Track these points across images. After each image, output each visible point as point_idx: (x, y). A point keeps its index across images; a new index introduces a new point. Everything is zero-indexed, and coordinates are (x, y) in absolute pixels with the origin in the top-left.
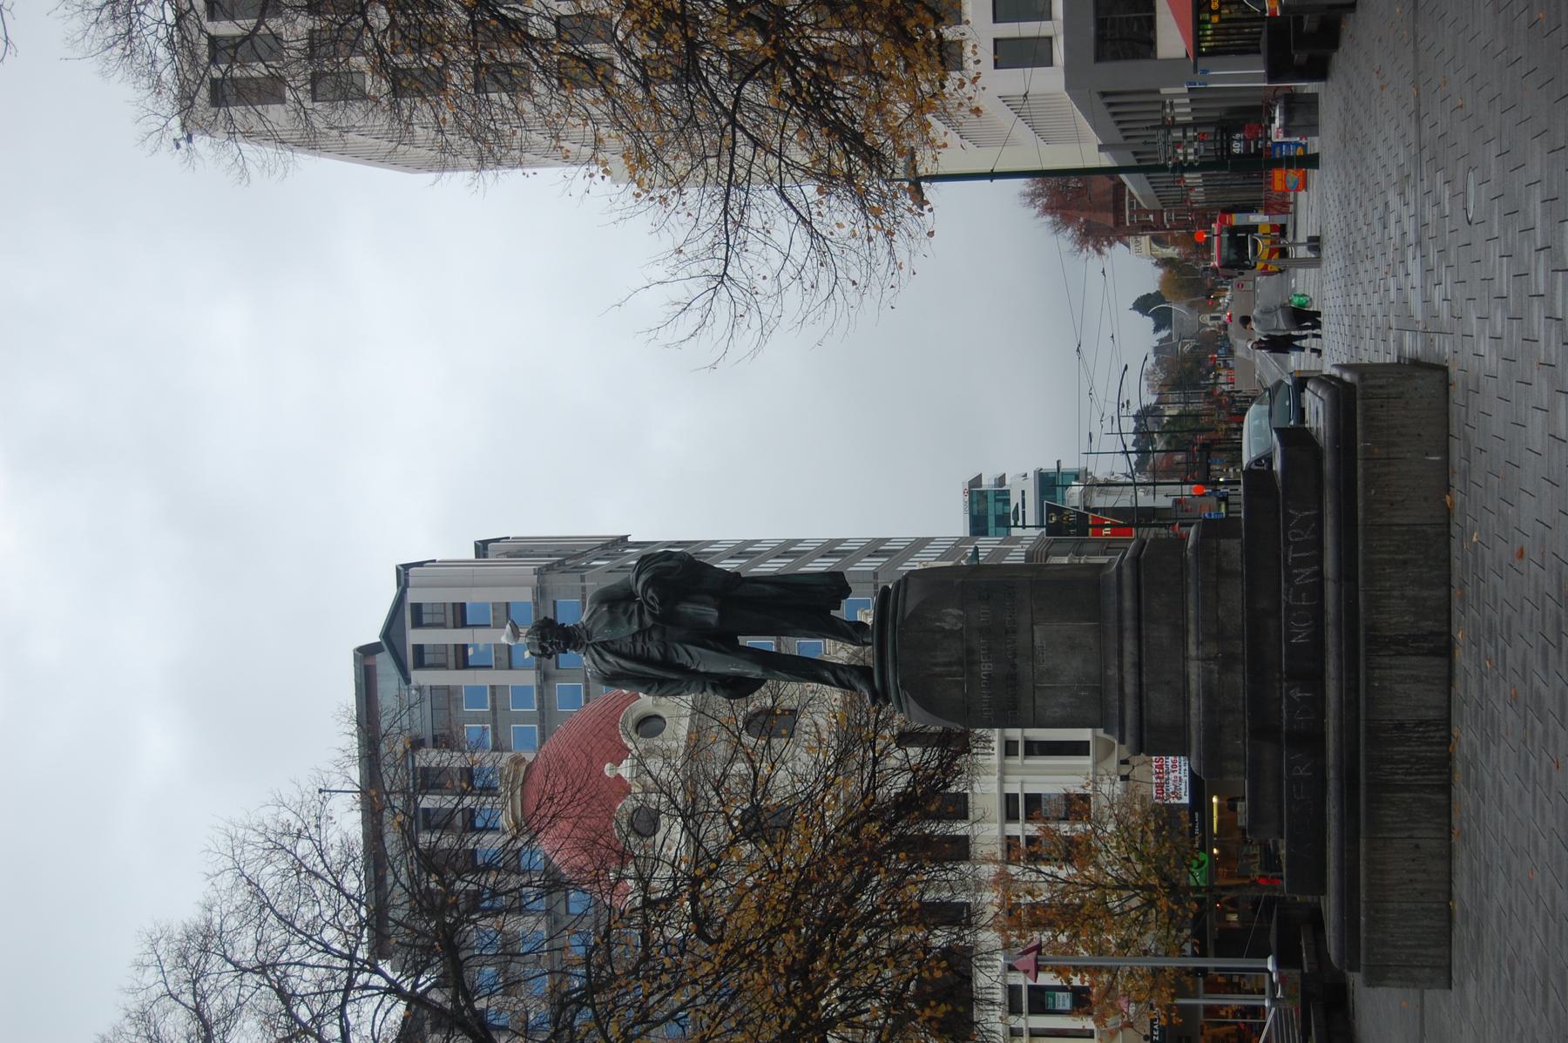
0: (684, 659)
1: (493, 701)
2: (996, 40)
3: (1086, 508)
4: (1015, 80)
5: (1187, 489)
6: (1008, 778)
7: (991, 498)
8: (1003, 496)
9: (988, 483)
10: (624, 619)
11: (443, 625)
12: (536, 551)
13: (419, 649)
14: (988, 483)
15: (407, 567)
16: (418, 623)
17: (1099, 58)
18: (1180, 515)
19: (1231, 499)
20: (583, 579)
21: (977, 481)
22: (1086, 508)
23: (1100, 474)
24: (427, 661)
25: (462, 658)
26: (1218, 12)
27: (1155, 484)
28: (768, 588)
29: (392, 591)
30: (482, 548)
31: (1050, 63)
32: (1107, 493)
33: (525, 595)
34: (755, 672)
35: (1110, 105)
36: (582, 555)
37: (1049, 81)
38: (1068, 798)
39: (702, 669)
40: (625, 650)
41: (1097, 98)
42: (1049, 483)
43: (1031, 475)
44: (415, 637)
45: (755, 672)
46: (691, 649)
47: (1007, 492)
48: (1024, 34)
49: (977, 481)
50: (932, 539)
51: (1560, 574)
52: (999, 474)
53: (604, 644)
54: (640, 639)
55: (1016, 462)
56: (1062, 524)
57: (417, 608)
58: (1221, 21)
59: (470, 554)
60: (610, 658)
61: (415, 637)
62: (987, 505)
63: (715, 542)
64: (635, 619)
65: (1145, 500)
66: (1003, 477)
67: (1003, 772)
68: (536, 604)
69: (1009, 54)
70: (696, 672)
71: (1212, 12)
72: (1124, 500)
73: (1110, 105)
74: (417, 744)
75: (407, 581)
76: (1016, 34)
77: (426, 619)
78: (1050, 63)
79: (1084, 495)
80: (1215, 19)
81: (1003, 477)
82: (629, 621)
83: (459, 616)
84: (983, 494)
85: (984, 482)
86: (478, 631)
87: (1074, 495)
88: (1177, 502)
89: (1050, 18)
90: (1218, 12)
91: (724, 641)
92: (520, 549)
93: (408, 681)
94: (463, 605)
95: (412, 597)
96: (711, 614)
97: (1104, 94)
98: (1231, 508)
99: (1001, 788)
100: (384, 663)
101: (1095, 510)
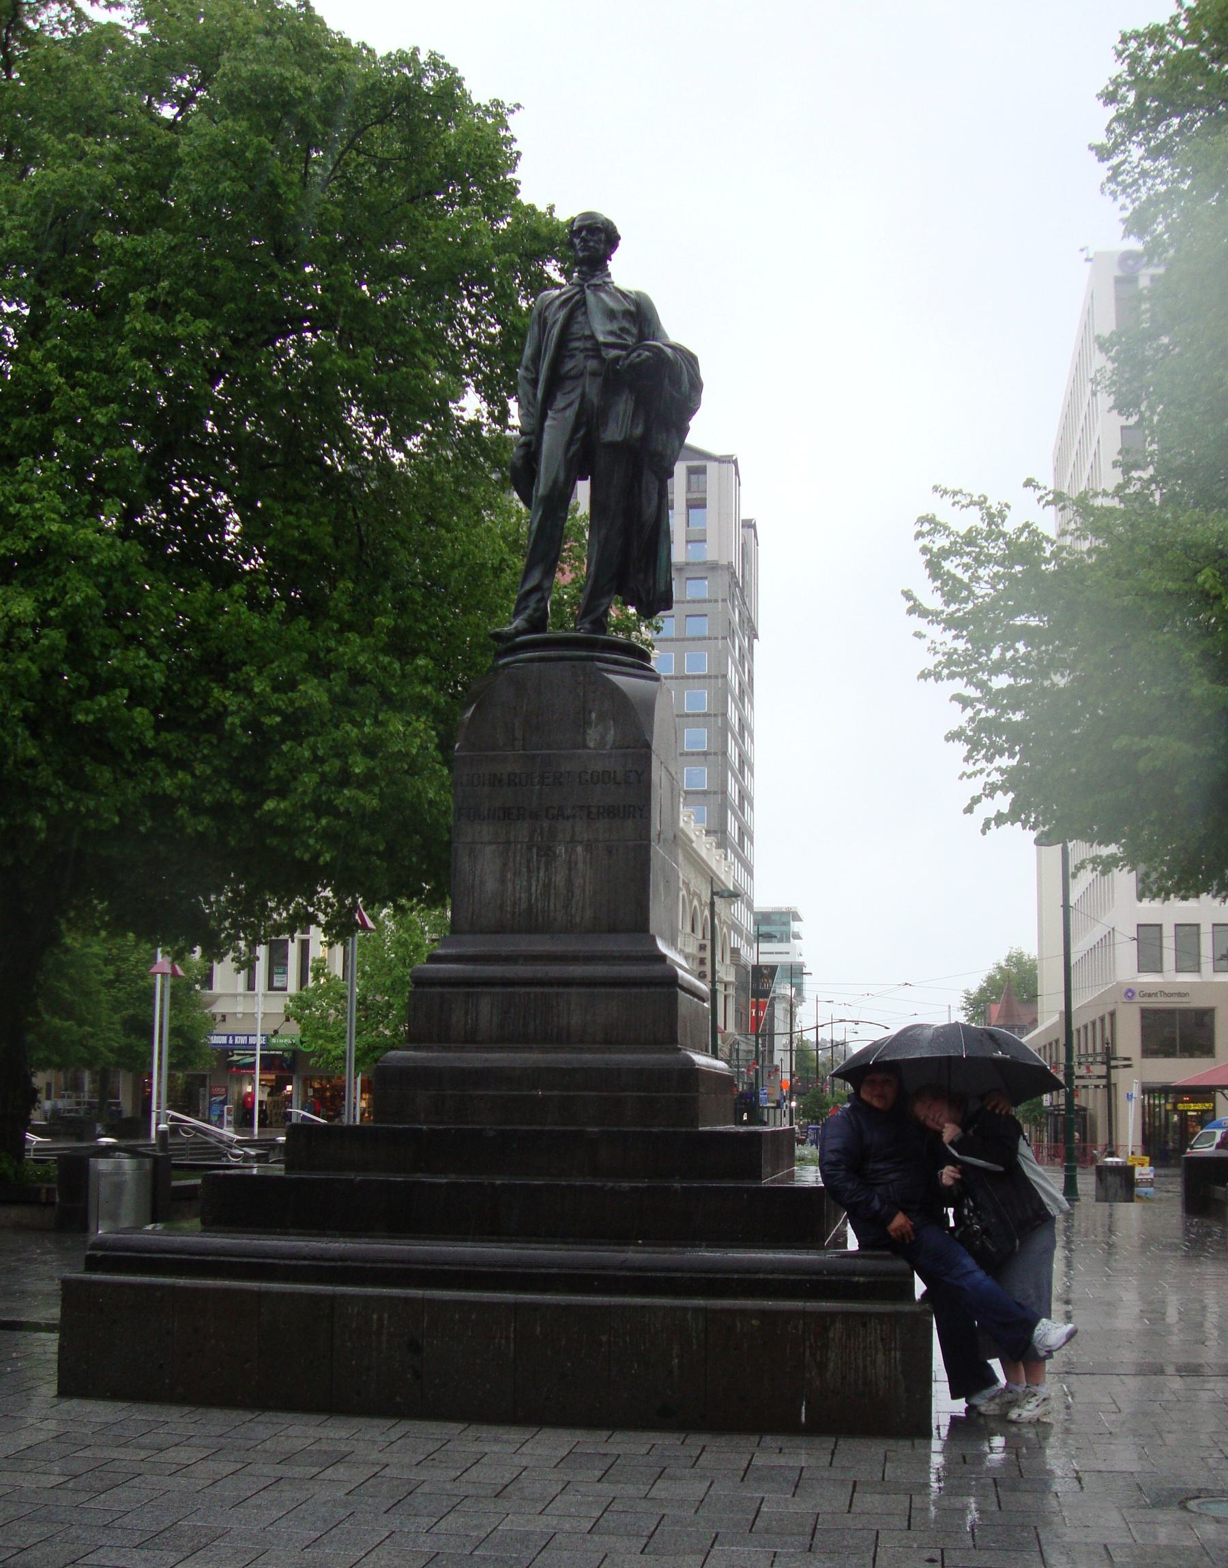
0: (560, 402)
2: (1160, 926)
3: (774, 998)
5: (786, 1077)
7: (784, 928)
8: (786, 937)
9: (795, 926)
10: (615, 327)
11: (689, 490)
12: (747, 567)
14: (795, 926)
15: (735, 463)
16: (691, 471)
18: (766, 1070)
19: (778, 1111)
20: (724, 600)
21: (797, 917)
22: (774, 998)
23: (800, 1011)
26: (1175, 1110)
27: (791, 1050)
28: (655, 502)
29: (717, 451)
30: (749, 525)
31: (1141, 969)
32: (785, 1017)
33: (710, 553)
34: (541, 488)
35: (1094, 1023)
36: (744, 603)
37: (1125, 966)
39: (548, 423)
40: (575, 328)
41: (1110, 1008)
42: (795, 973)
43: (800, 959)
45: (541, 488)
46: (576, 406)
47: (788, 941)
48: (1165, 951)
49: (797, 917)
50: (752, 878)
52: (801, 914)
53: (583, 303)
54: (589, 345)
55: (808, 948)
56: (759, 981)
57: (701, 471)
58: (1167, 1111)
59: (744, 515)
60: (562, 315)
62: (774, 926)
63: (752, 707)
64: (611, 339)
65: (781, 1042)
66: (800, 938)
68: (705, 563)
69: (1148, 936)
70: (543, 417)
71: (1175, 1105)
72: (780, 1026)
73: (1094, 1023)
75: (724, 462)
77: (694, 477)
78: (1141, 969)
79: (784, 997)
80: (1169, 1107)
81: (800, 938)
82: (611, 333)
83: (696, 504)
84: (787, 924)
85: (797, 923)
86: (684, 517)
87: (783, 989)
88: (776, 1069)
89: (1177, 971)
90: (1175, 1110)
91: (582, 461)
92: (747, 554)
94: (704, 506)
95: (711, 467)
96: (613, 433)
97: (1112, 1014)
98: (771, 1111)
101: (772, 1006)
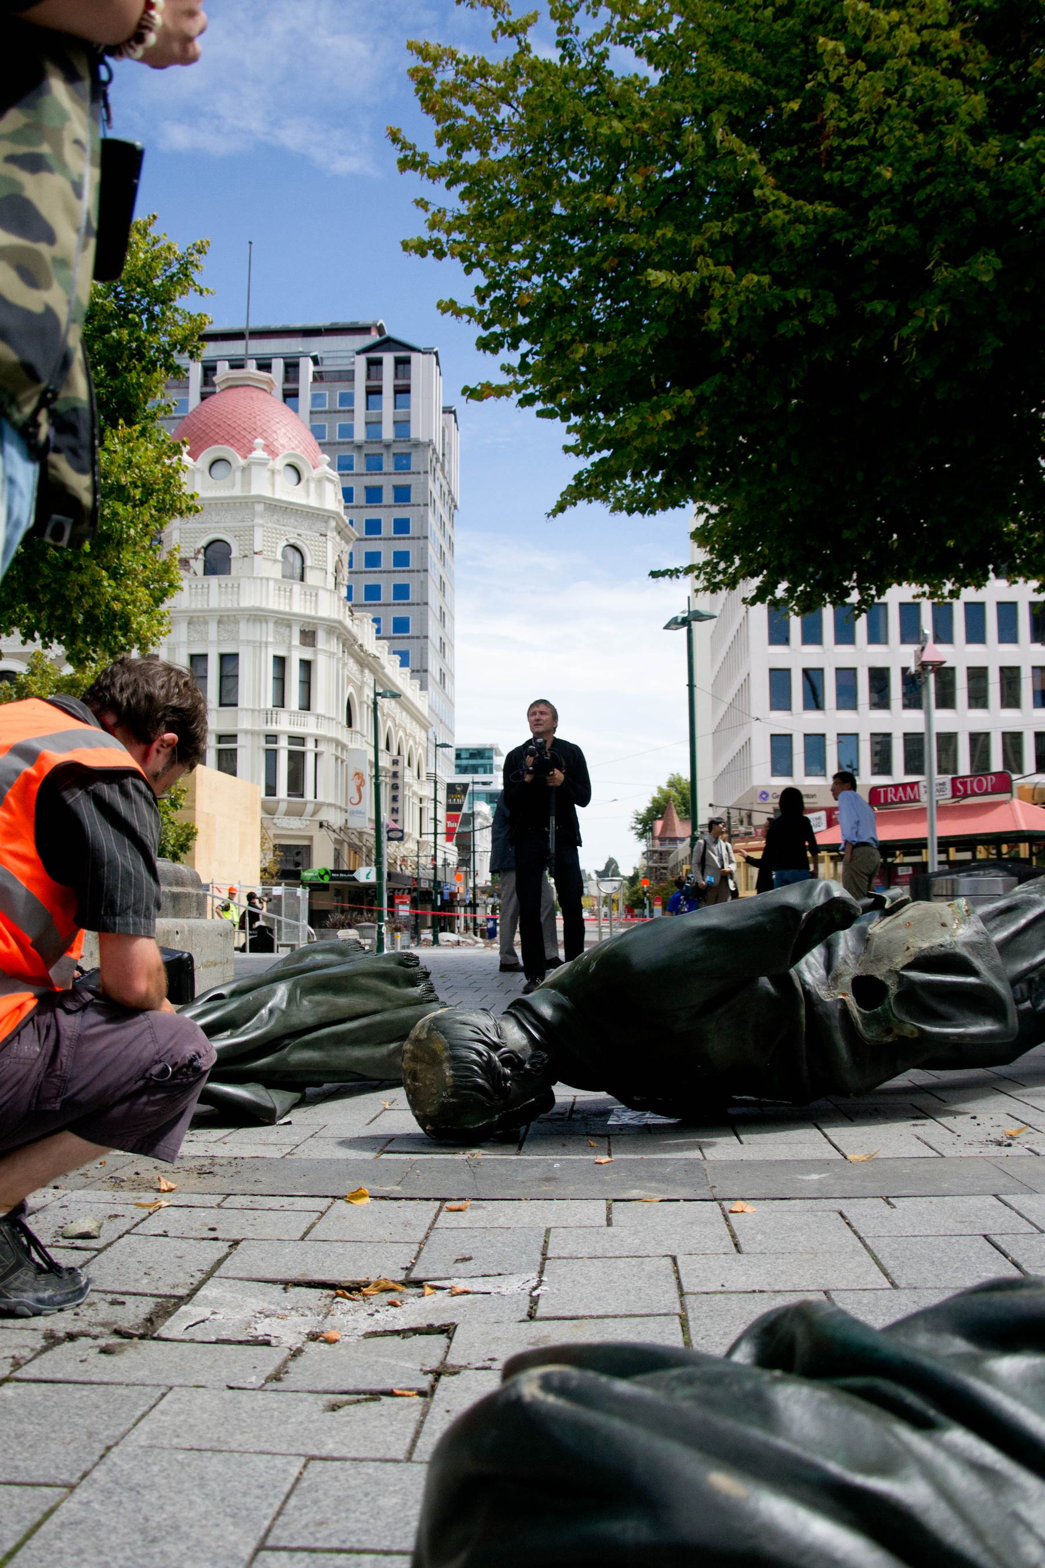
1: (343, 443)
4: (762, 754)
6: (249, 736)
13: (379, 362)
17: (968, 668)
24: (371, 397)
25: (374, 391)
38: (162, 602)
44: (388, 359)
51: (141, 1034)
57: (407, 361)
61: (388, 359)
67: (253, 733)
74: (316, 361)
76: (802, 756)
77: (400, 367)
83: (402, 391)
93: (358, 353)
95: (415, 357)
99: (246, 732)
100: (374, 337)
